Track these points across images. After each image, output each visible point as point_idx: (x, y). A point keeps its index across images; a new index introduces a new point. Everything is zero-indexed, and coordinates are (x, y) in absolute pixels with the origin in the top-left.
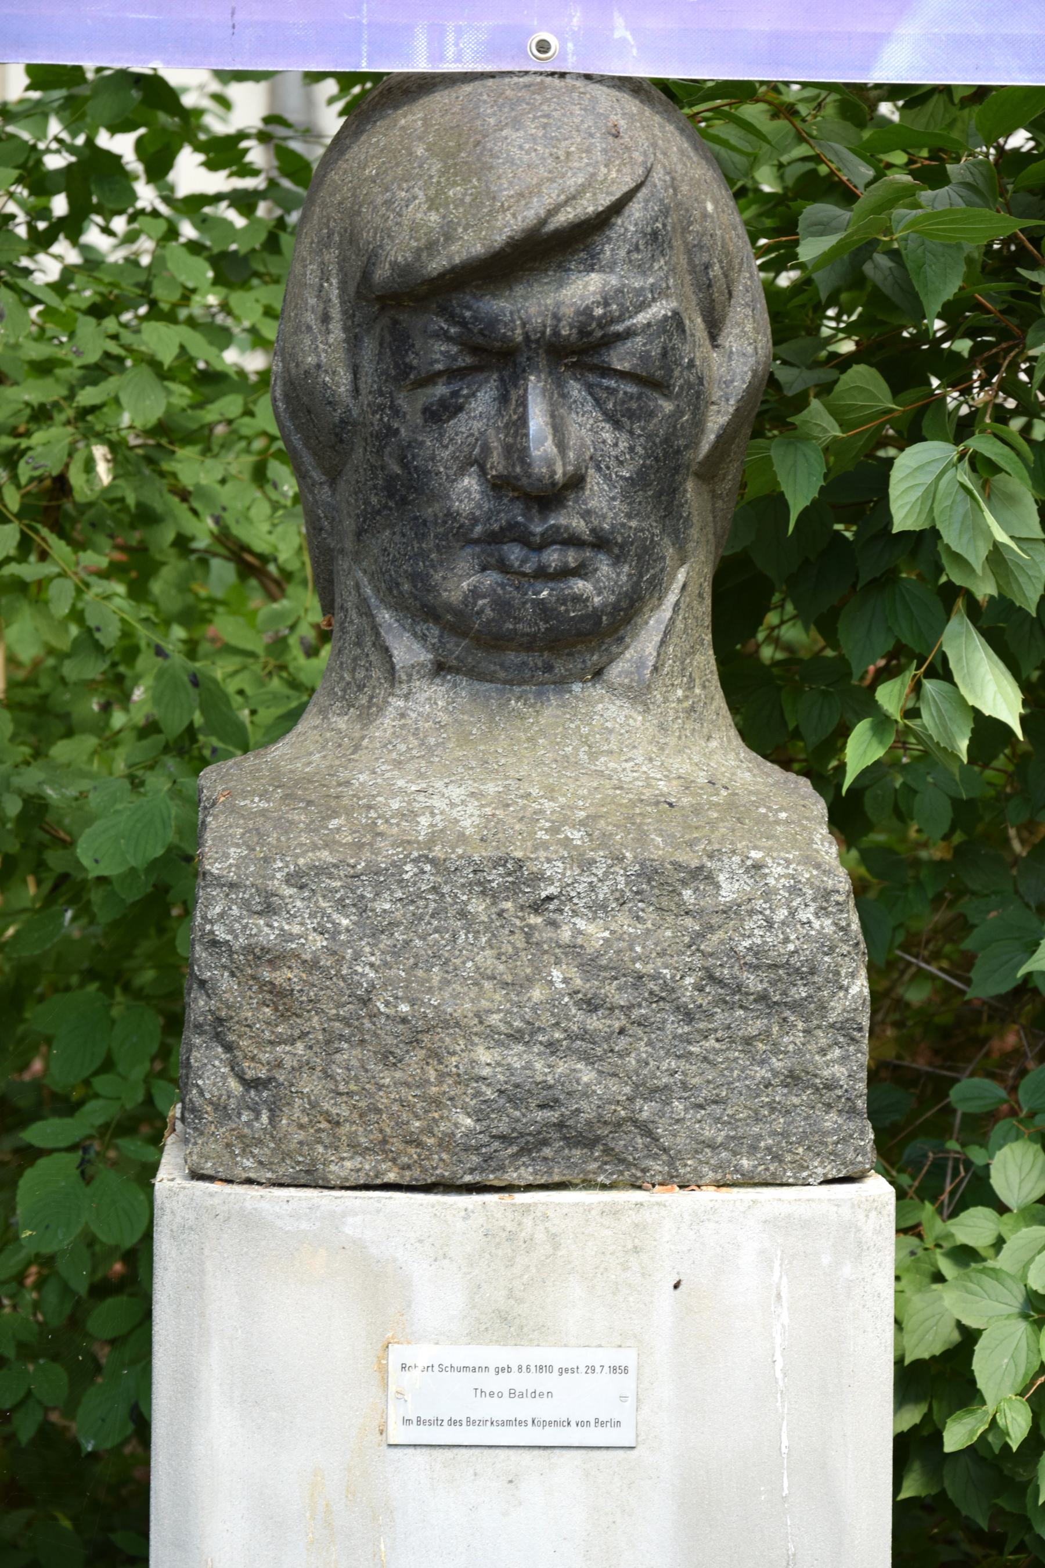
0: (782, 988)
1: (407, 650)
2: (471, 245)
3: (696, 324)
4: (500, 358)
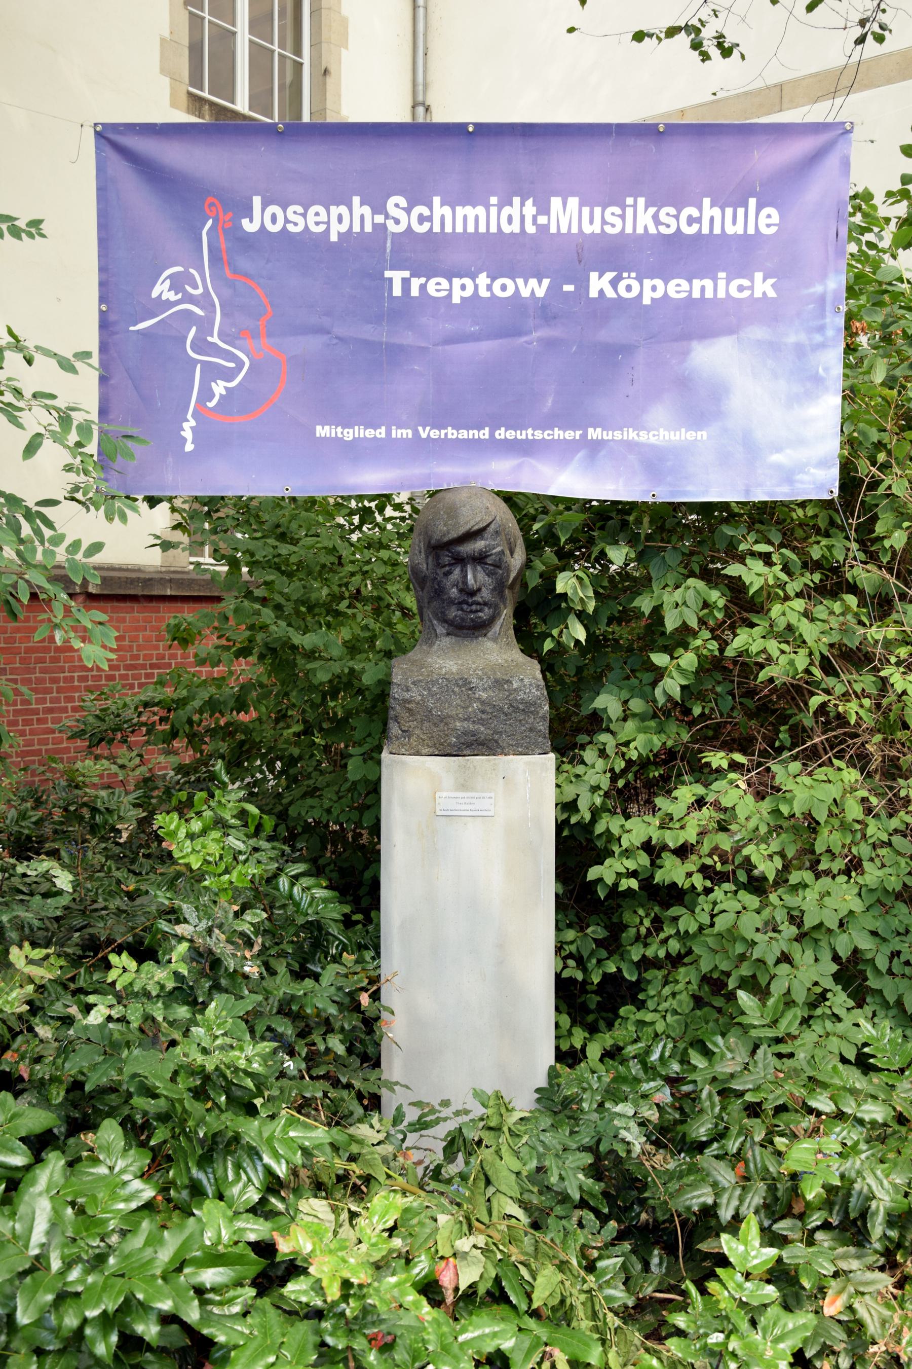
0: (529, 708)
1: (441, 629)
2: (454, 535)
3: (508, 552)
4: (461, 561)
